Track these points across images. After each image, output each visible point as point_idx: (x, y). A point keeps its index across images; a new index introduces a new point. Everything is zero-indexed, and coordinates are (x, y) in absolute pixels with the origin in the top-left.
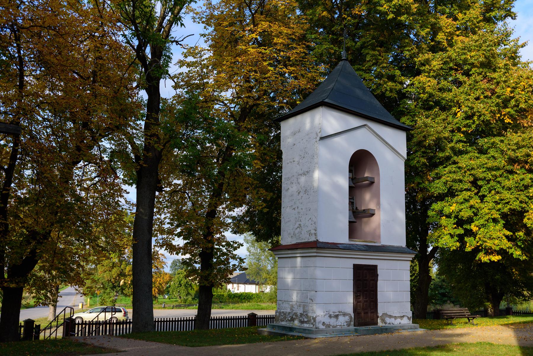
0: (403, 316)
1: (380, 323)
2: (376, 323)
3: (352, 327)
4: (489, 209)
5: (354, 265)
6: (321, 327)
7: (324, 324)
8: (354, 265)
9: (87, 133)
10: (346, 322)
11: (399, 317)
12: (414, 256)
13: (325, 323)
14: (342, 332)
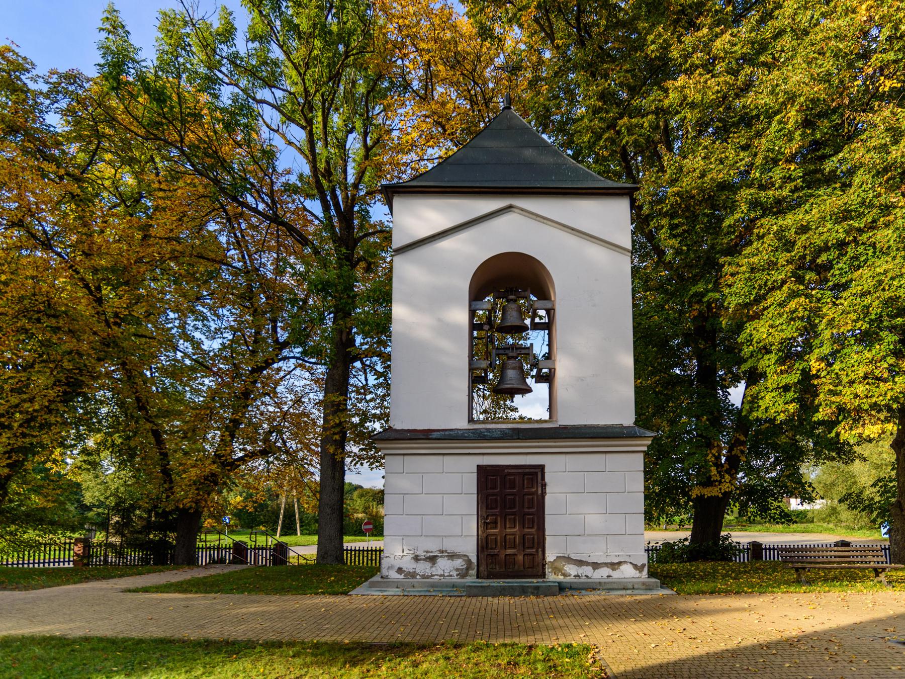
0: (620, 563)
1: (552, 577)
2: (543, 575)
3: (471, 579)
4: (49, 401)
5: (479, 467)
6: (394, 575)
7: (400, 570)
8: (479, 467)
9: (86, 185)
10: (457, 570)
11: (605, 564)
12: (650, 442)
13: (404, 569)
14: (451, 589)
